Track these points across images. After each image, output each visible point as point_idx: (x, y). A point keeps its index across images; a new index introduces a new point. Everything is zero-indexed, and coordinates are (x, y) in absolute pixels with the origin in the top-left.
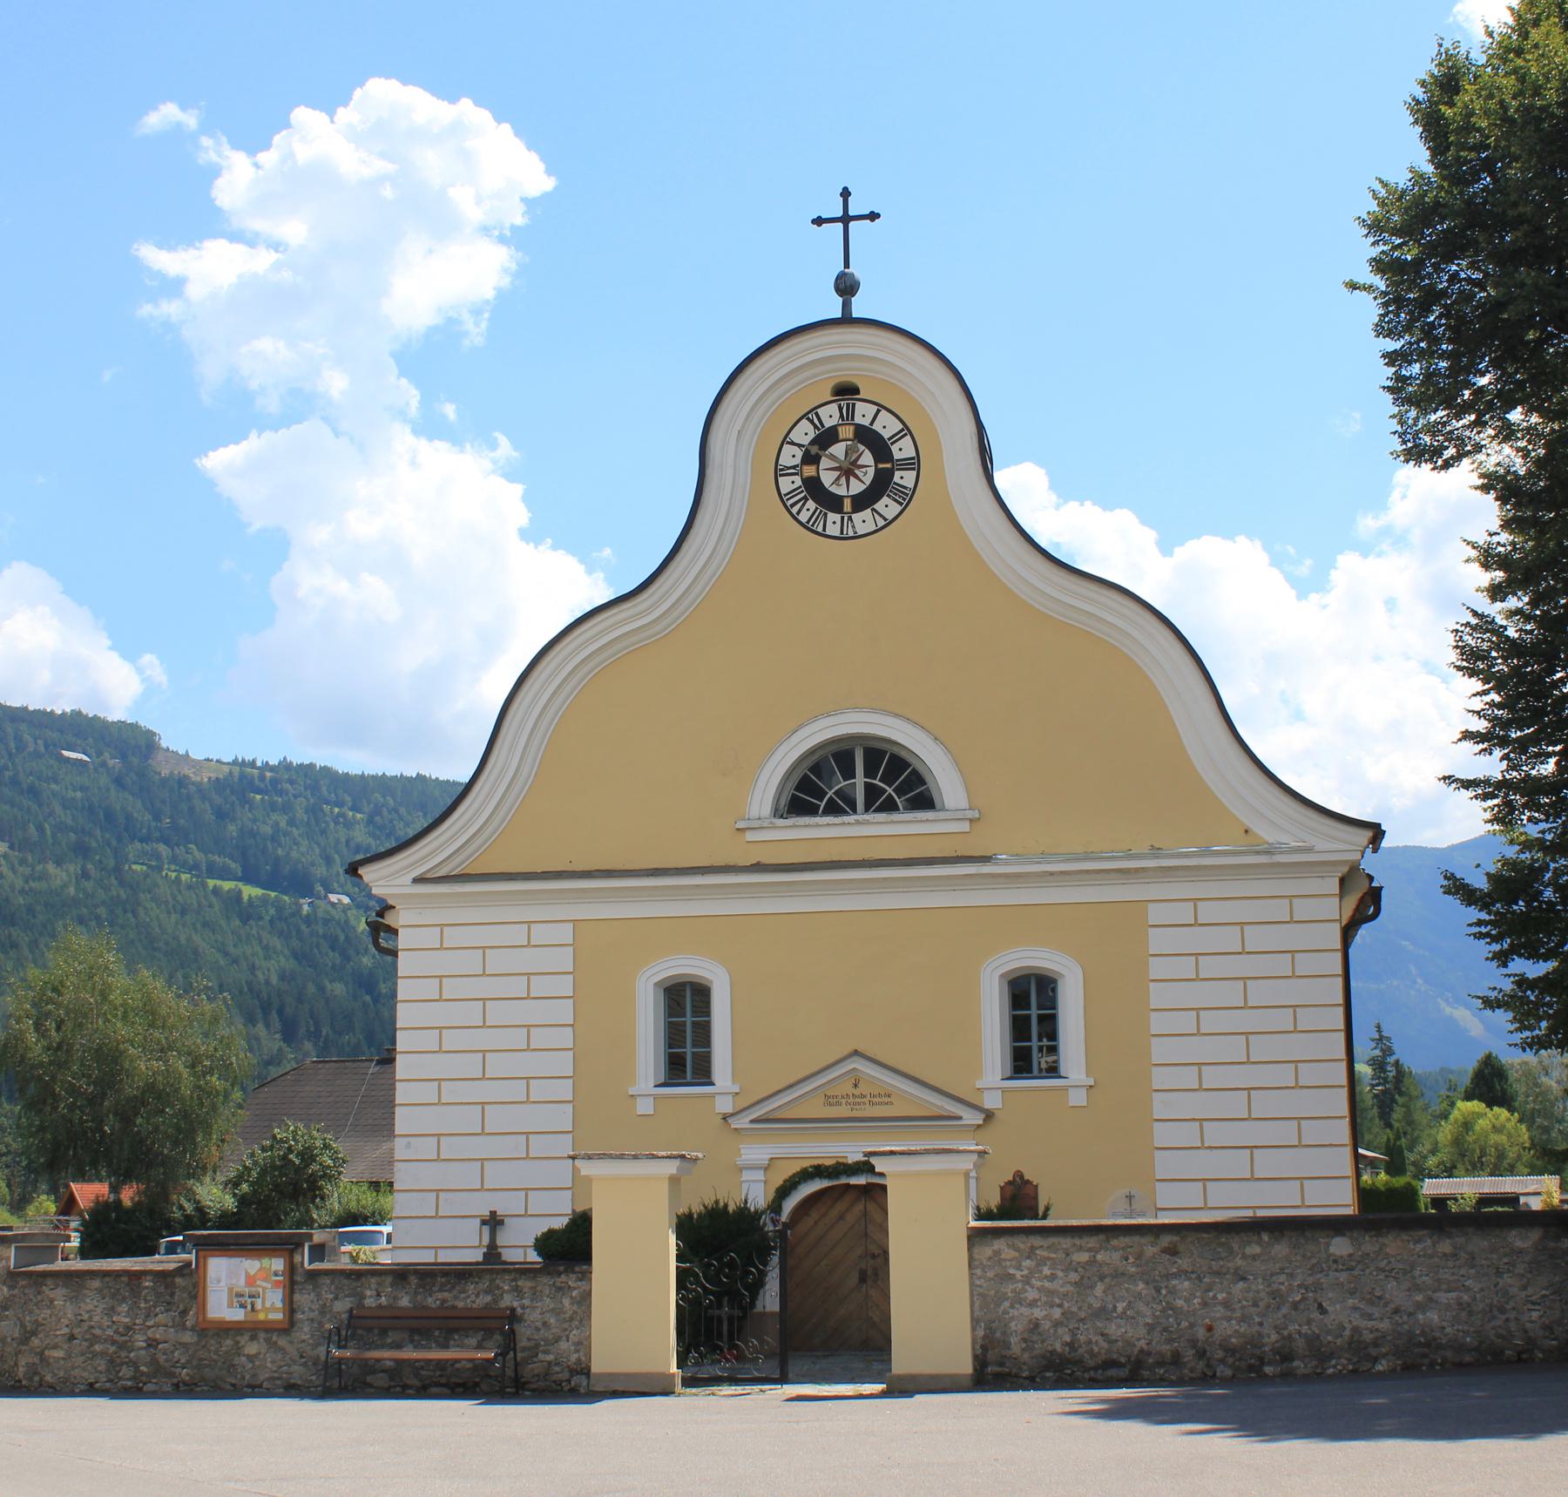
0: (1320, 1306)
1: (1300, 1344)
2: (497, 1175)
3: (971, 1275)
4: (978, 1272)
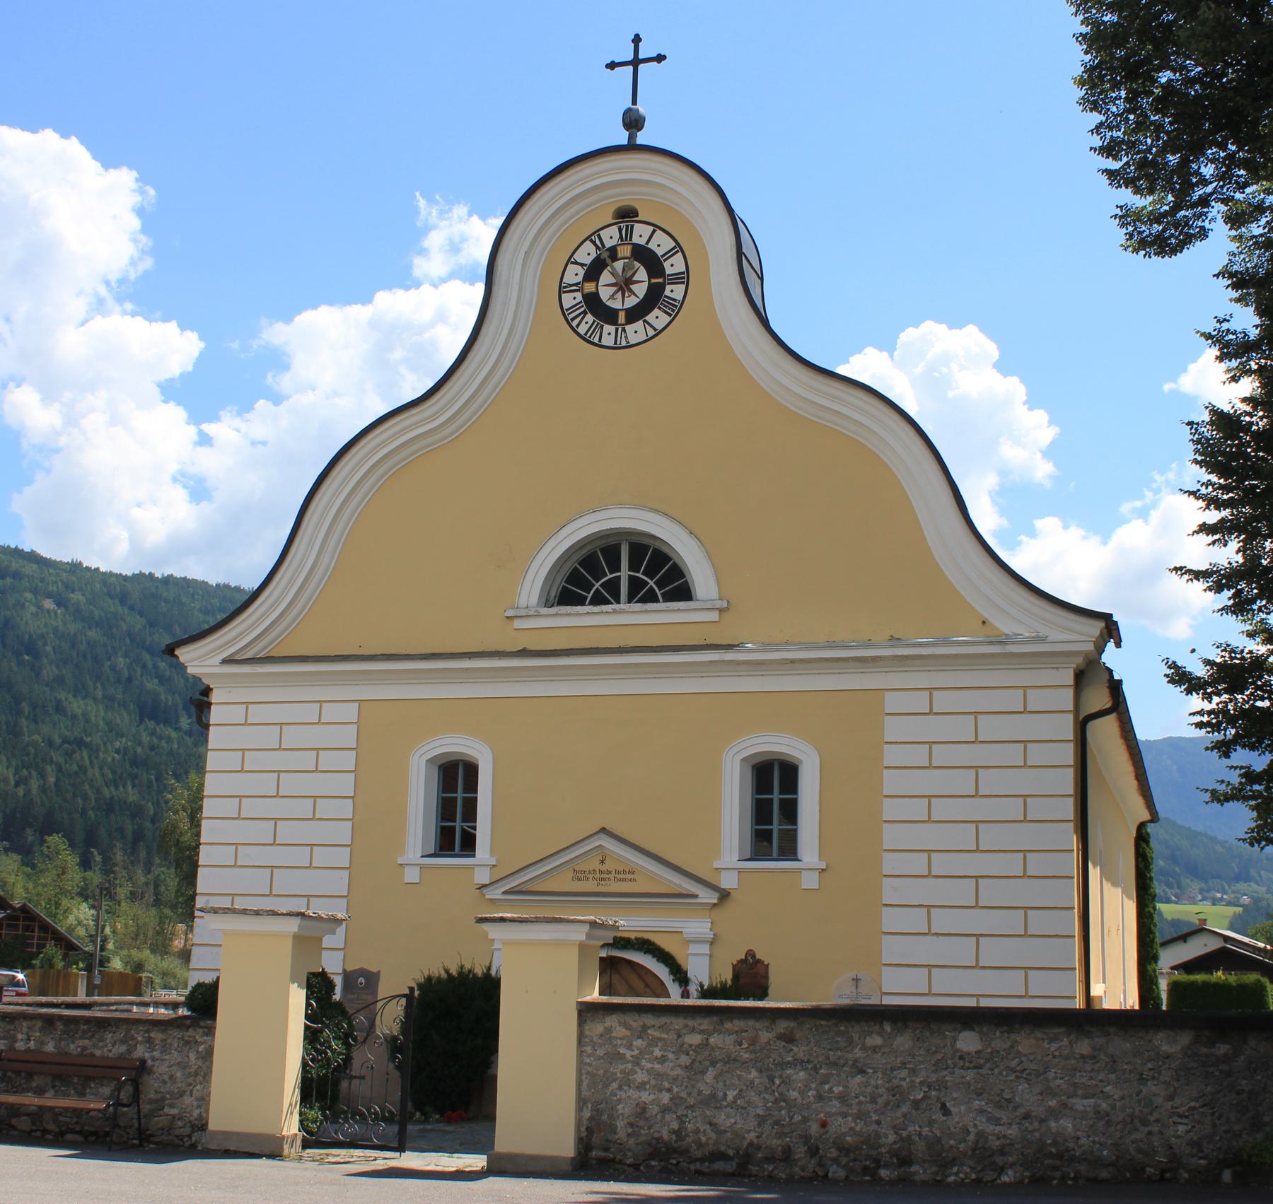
0: (943, 1106)
1: (920, 1147)
3: (581, 1053)
4: (589, 1049)
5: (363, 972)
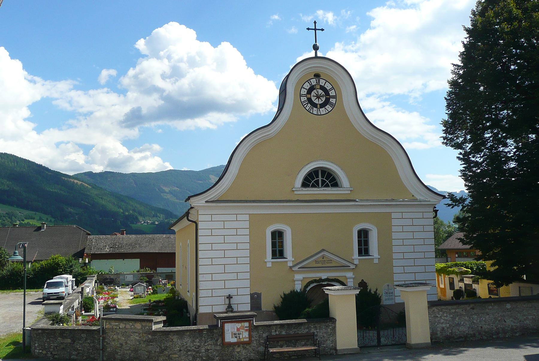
2: (229, 284)
5: (256, 293)
